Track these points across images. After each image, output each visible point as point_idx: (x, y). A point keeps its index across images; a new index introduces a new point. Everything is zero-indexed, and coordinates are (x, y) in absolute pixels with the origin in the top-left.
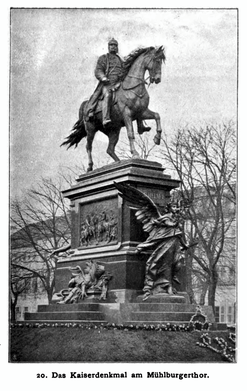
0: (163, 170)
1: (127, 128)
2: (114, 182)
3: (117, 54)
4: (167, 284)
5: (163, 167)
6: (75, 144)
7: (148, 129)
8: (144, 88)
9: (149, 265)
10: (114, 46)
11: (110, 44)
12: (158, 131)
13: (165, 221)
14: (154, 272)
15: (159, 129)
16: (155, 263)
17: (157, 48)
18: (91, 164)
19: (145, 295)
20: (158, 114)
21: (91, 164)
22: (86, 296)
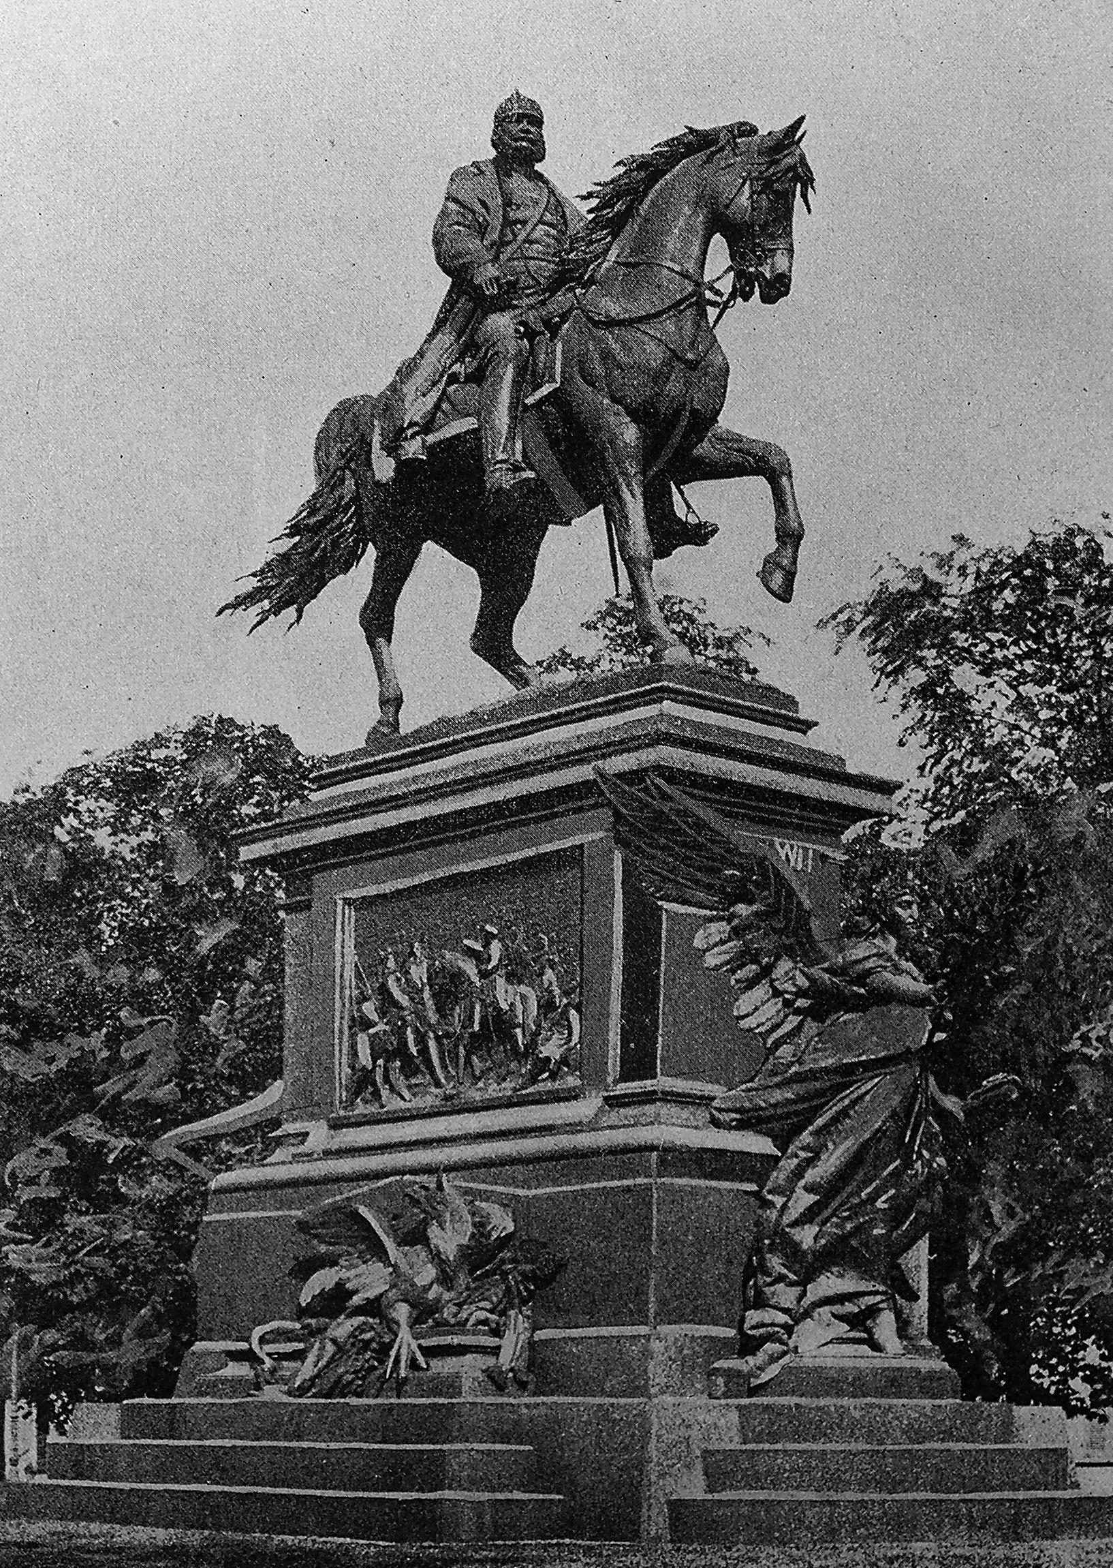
0: (806, 726)
1: (616, 520)
2: (598, 771)
3: (538, 167)
4: (870, 1300)
5: (802, 716)
6: (291, 611)
7: (700, 534)
8: (704, 332)
9: (779, 1201)
10: (524, 124)
11: (501, 119)
12: (383, 703)
13: (869, 972)
14: (806, 1237)
15: (391, 693)
16: (809, 1189)
17: (770, 124)
18: (392, 702)
19: (761, 1358)
20: (780, 452)
21: (392, 702)
22: (421, 1360)
